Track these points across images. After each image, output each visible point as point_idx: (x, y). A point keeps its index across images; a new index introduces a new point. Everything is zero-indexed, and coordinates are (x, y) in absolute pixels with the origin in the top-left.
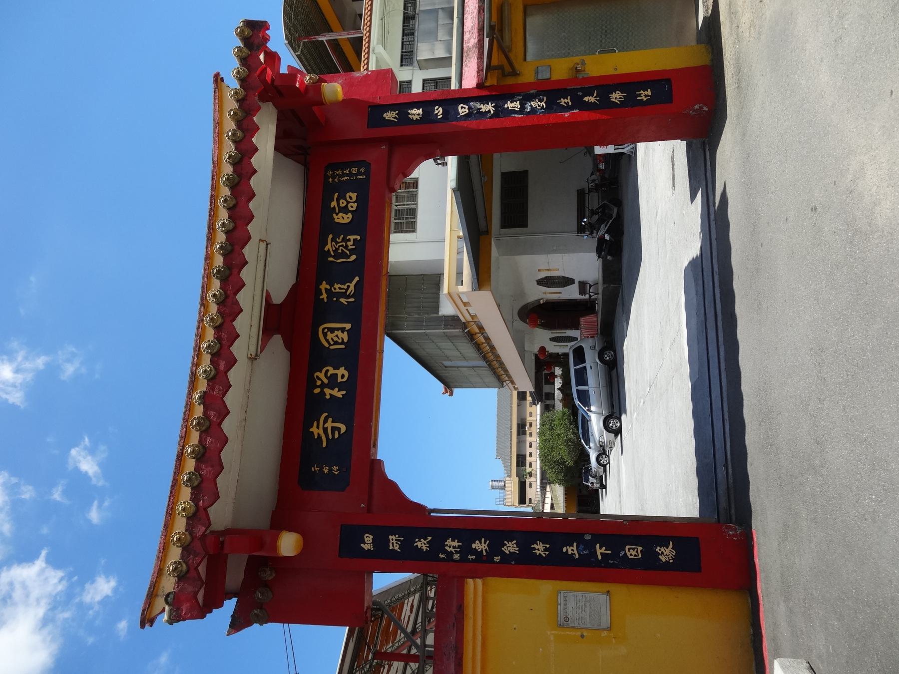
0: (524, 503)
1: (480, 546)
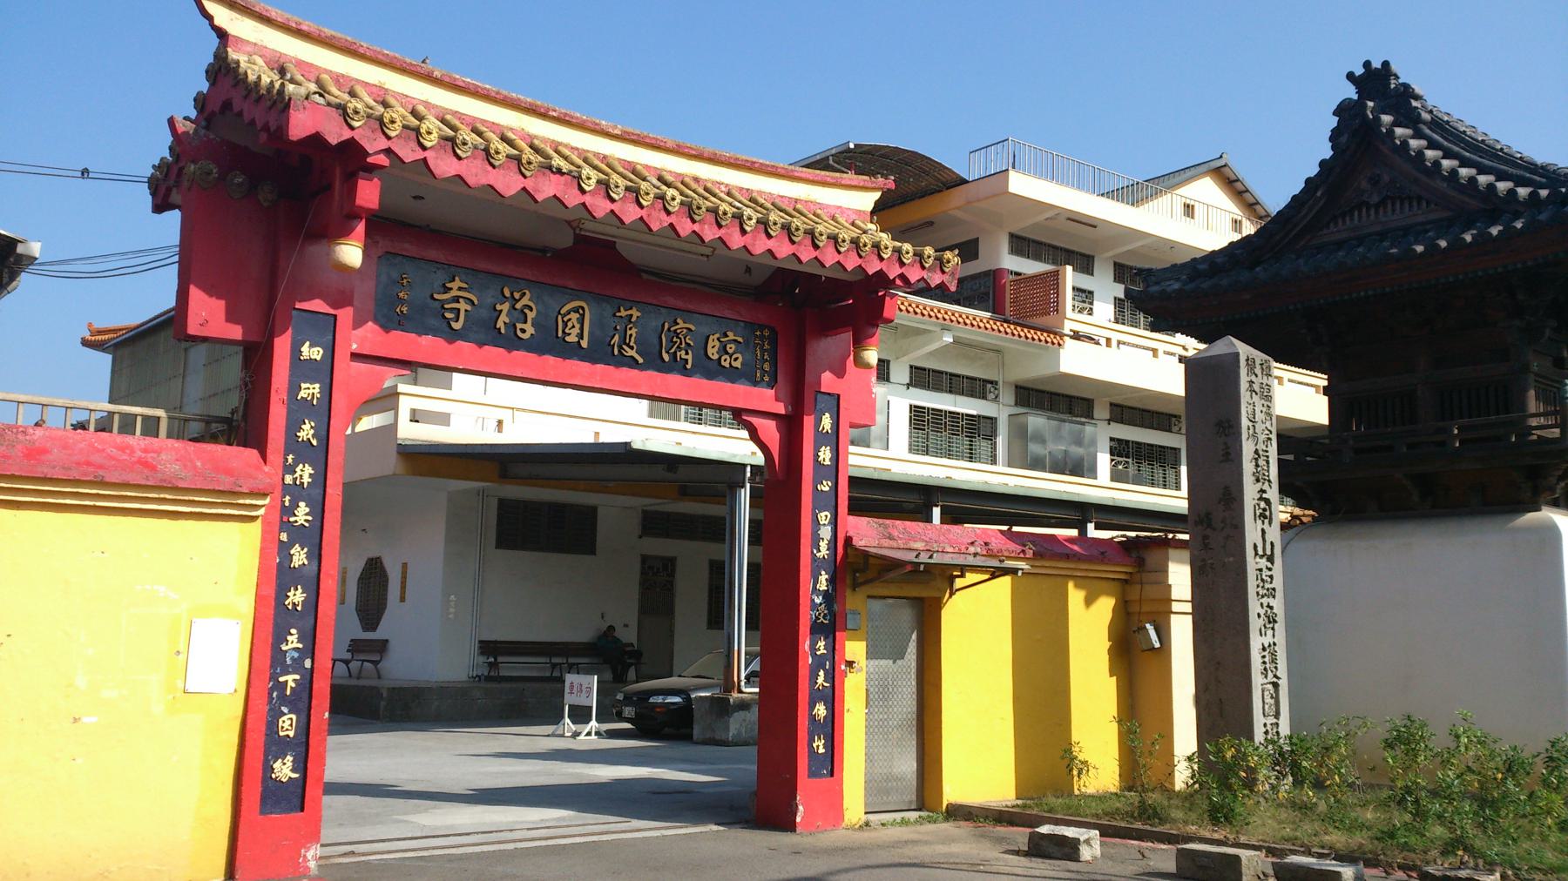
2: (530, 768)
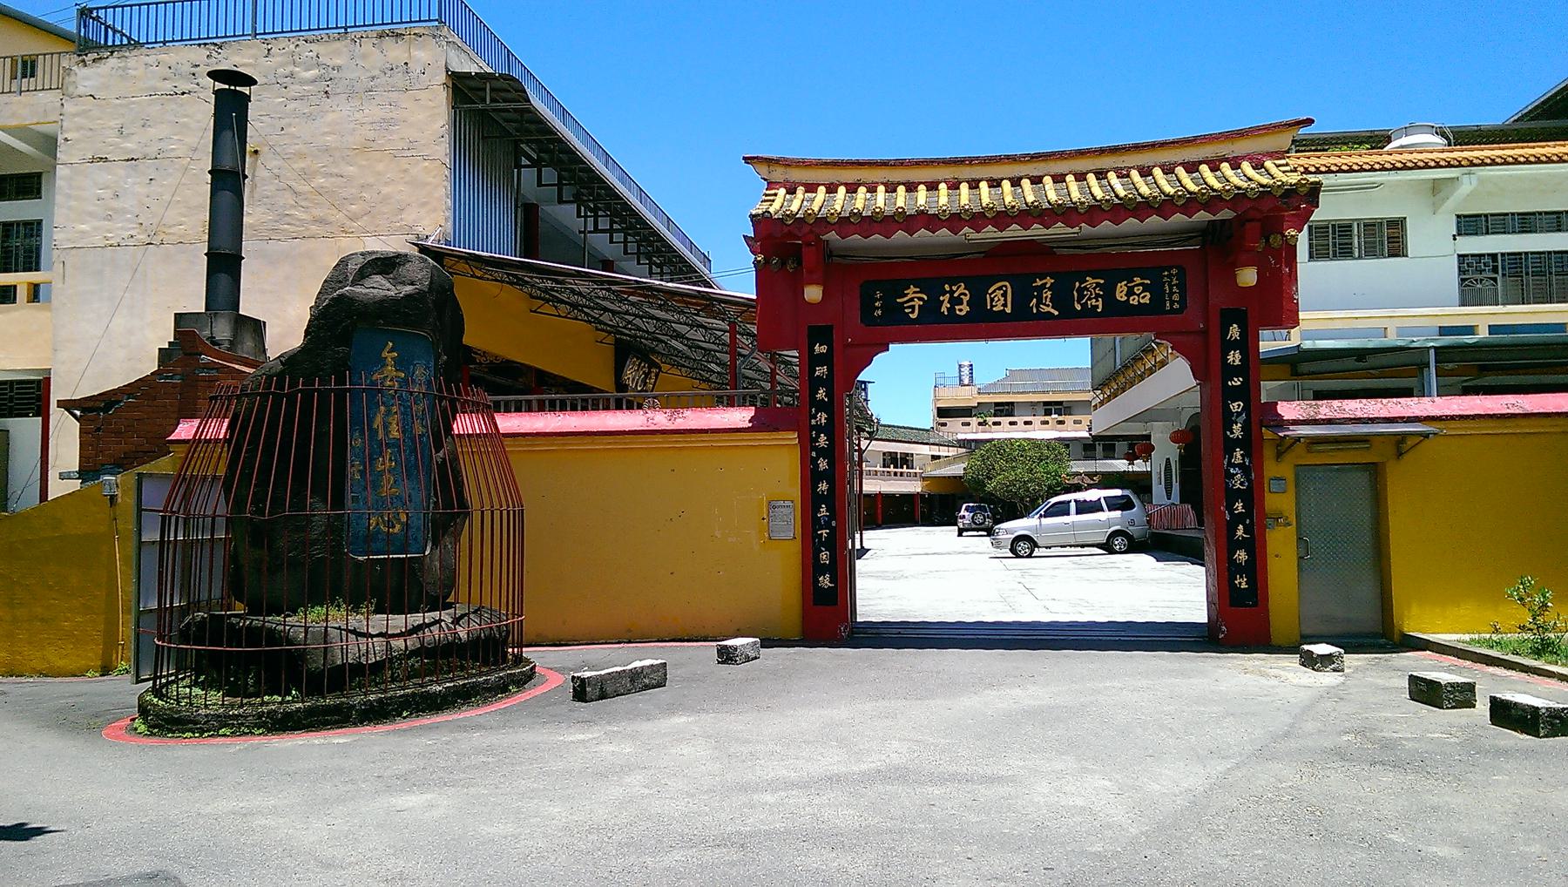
0: (940, 416)
1: (823, 441)
2: (1166, 574)
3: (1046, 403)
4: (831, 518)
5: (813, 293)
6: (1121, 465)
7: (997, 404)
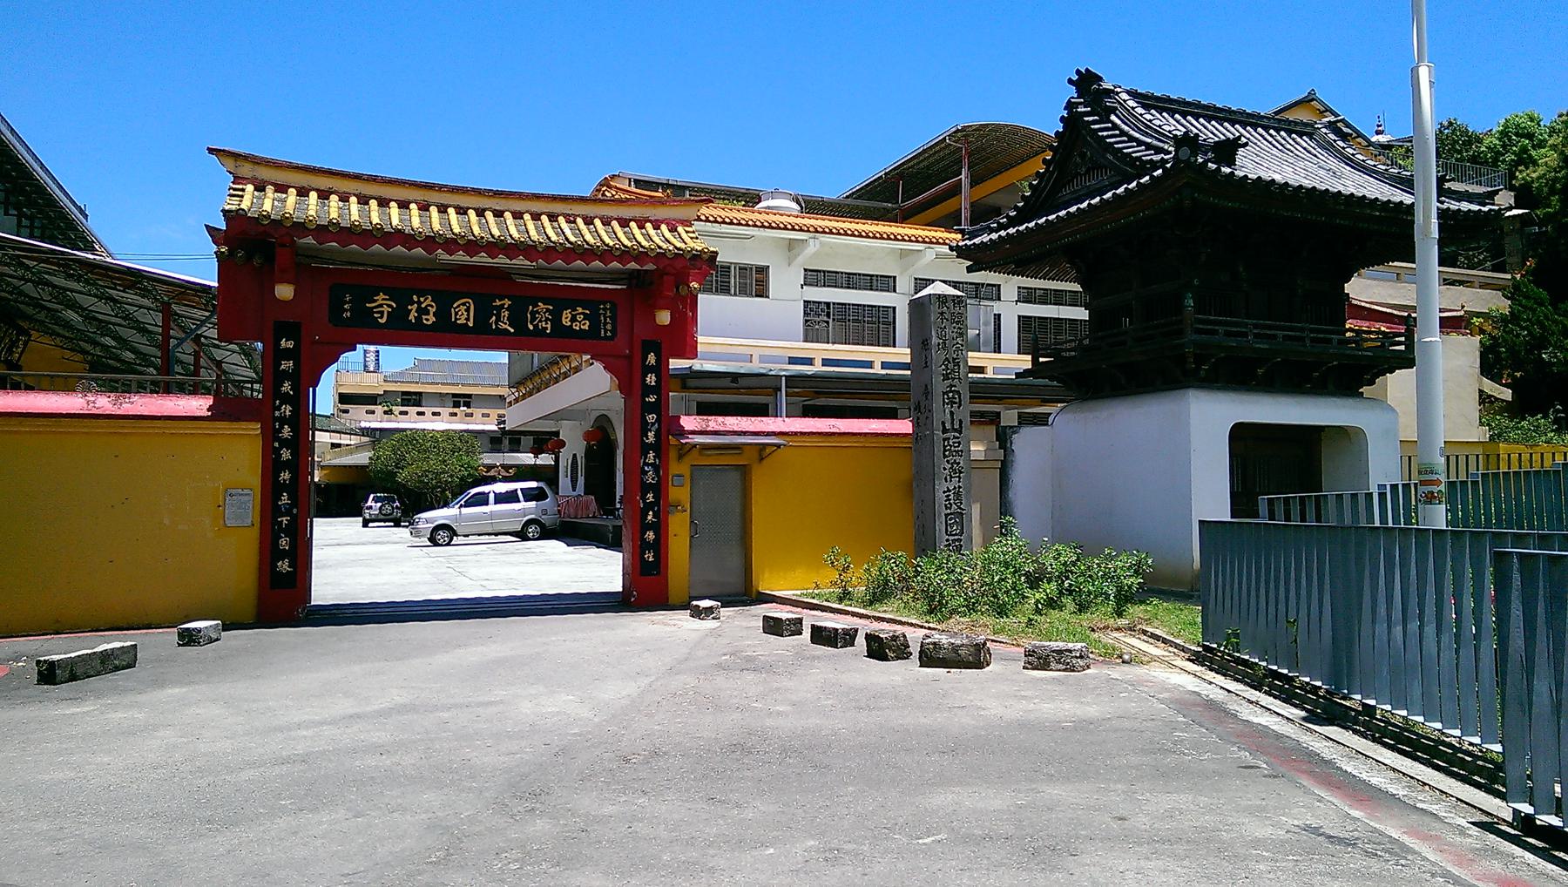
3: (454, 395)
4: (292, 506)
5: (285, 291)
6: (527, 458)
7: (404, 393)
